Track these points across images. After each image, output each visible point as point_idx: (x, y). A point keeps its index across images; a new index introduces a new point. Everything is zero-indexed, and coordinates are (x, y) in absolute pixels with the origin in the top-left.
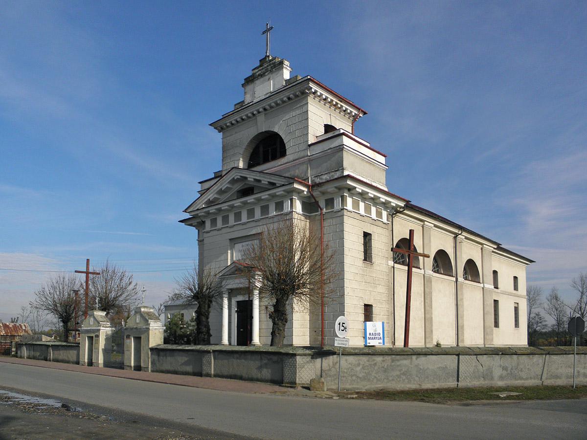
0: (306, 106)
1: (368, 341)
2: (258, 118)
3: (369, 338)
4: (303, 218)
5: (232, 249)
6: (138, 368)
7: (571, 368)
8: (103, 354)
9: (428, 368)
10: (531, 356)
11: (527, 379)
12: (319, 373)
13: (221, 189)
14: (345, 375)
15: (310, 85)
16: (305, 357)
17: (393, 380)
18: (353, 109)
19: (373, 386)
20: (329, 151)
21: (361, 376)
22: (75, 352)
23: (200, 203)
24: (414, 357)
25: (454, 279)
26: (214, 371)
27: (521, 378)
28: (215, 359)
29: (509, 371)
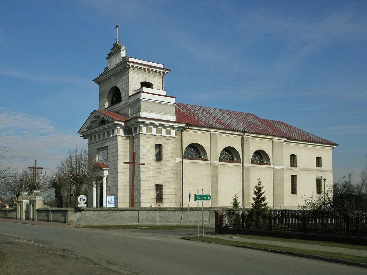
0: (124, 78)
1: (108, 205)
2: (112, 78)
3: (108, 204)
4: (124, 138)
5: (98, 155)
6: (33, 219)
7: (196, 217)
8: (25, 213)
9: (125, 217)
10: (175, 212)
11: (173, 222)
12: (78, 218)
13: (87, 126)
14: (89, 219)
15: (128, 64)
16: (72, 212)
17: (109, 221)
18: (161, 69)
19: (100, 224)
20: (136, 101)
21: (95, 220)
22: (16, 213)
23: (84, 128)
24: (118, 212)
25: (241, 164)
26: (52, 219)
27: (170, 222)
28: (52, 213)
29: (164, 219)
